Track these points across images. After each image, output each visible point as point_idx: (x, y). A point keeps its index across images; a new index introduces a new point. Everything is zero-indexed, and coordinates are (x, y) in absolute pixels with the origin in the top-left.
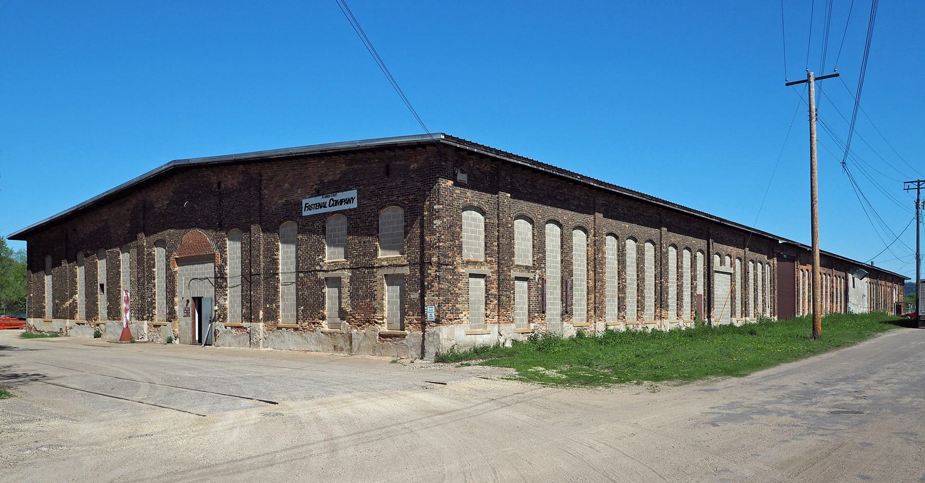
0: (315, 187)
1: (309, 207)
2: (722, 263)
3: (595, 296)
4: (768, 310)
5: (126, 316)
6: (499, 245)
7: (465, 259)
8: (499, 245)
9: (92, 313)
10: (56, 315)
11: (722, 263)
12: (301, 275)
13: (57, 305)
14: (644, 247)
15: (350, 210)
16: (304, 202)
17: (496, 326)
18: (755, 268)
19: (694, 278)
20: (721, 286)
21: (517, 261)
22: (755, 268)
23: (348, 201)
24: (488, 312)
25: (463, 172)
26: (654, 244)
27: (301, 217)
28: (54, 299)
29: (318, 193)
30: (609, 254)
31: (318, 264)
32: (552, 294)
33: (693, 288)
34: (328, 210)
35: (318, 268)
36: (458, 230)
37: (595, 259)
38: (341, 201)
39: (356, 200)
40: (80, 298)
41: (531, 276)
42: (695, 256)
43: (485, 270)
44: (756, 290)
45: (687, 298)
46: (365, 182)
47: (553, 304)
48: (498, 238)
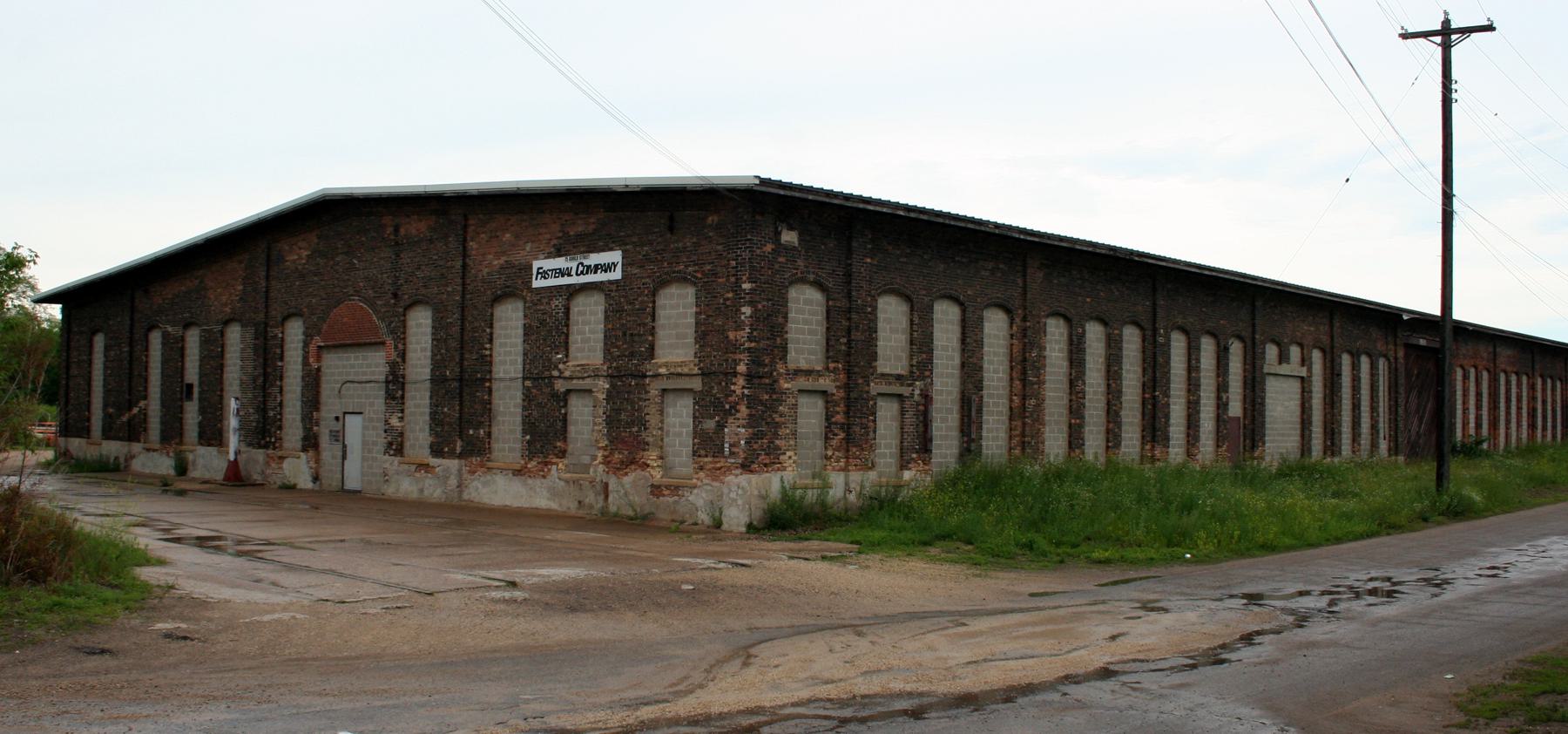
0: (555, 242)
1: (544, 274)
2: (1283, 358)
3: (1024, 424)
4: (1383, 446)
5: (233, 441)
6: (850, 341)
7: (792, 366)
8: (850, 341)
9: (172, 432)
10: (108, 433)
11: (1283, 358)
12: (528, 383)
13: (111, 416)
14: (1121, 336)
15: (610, 282)
16: (536, 264)
17: (842, 474)
18: (1355, 367)
19: (1222, 387)
20: (1281, 402)
21: (883, 366)
22: (1355, 367)
23: (607, 268)
24: (830, 453)
25: (791, 228)
26: (1141, 328)
27: (530, 289)
28: (106, 406)
29: (559, 253)
30: (1052, 350)
31: (556, 367)
32: (944, 420)
33: (1222, 405)
34: (574, 280)
35: (555, 373)
36: (781, 320)
37: (1025, 360)
38: (596, 266)
39: (619, 267)
40: (154, 405)
41: (905, 391)
42: (1226, 349)
43: (826, 383)
44: (1356, 407)
45: (1207, 424)
46: (635, 239)
47: (946, 437)
48: (849, 331)
